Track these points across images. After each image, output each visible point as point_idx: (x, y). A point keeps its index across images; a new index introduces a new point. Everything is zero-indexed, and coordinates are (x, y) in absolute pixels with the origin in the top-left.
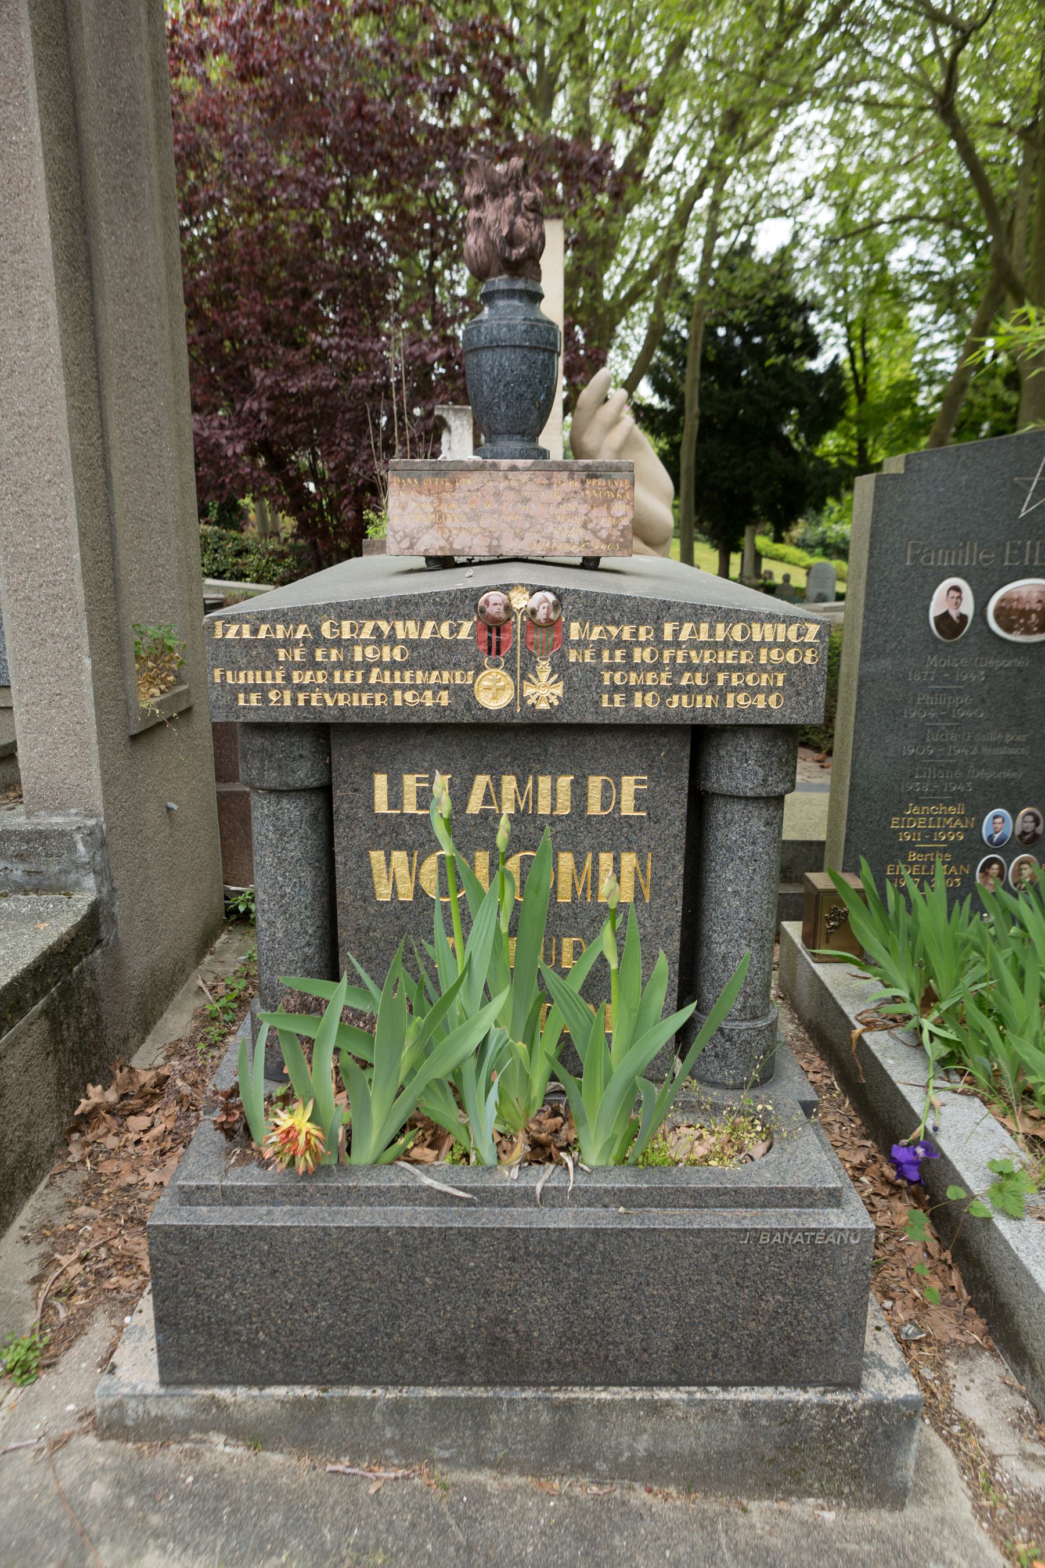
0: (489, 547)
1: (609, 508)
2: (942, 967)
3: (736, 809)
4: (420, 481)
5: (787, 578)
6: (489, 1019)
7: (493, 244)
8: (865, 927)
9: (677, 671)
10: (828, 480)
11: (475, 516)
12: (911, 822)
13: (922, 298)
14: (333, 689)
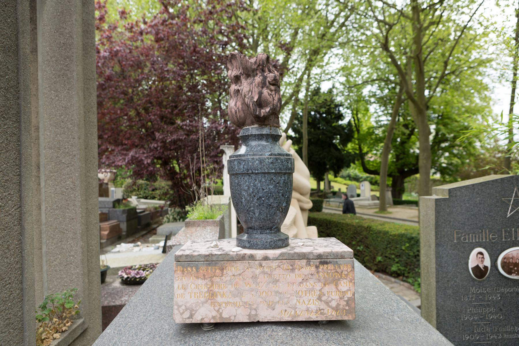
0: (249, 315)
1: (337, 285)
4: (197, 269)
5: (340, 190)
7: (248, 106)
10: (351, 158)
11: (239, 294)
13: (374, 102)
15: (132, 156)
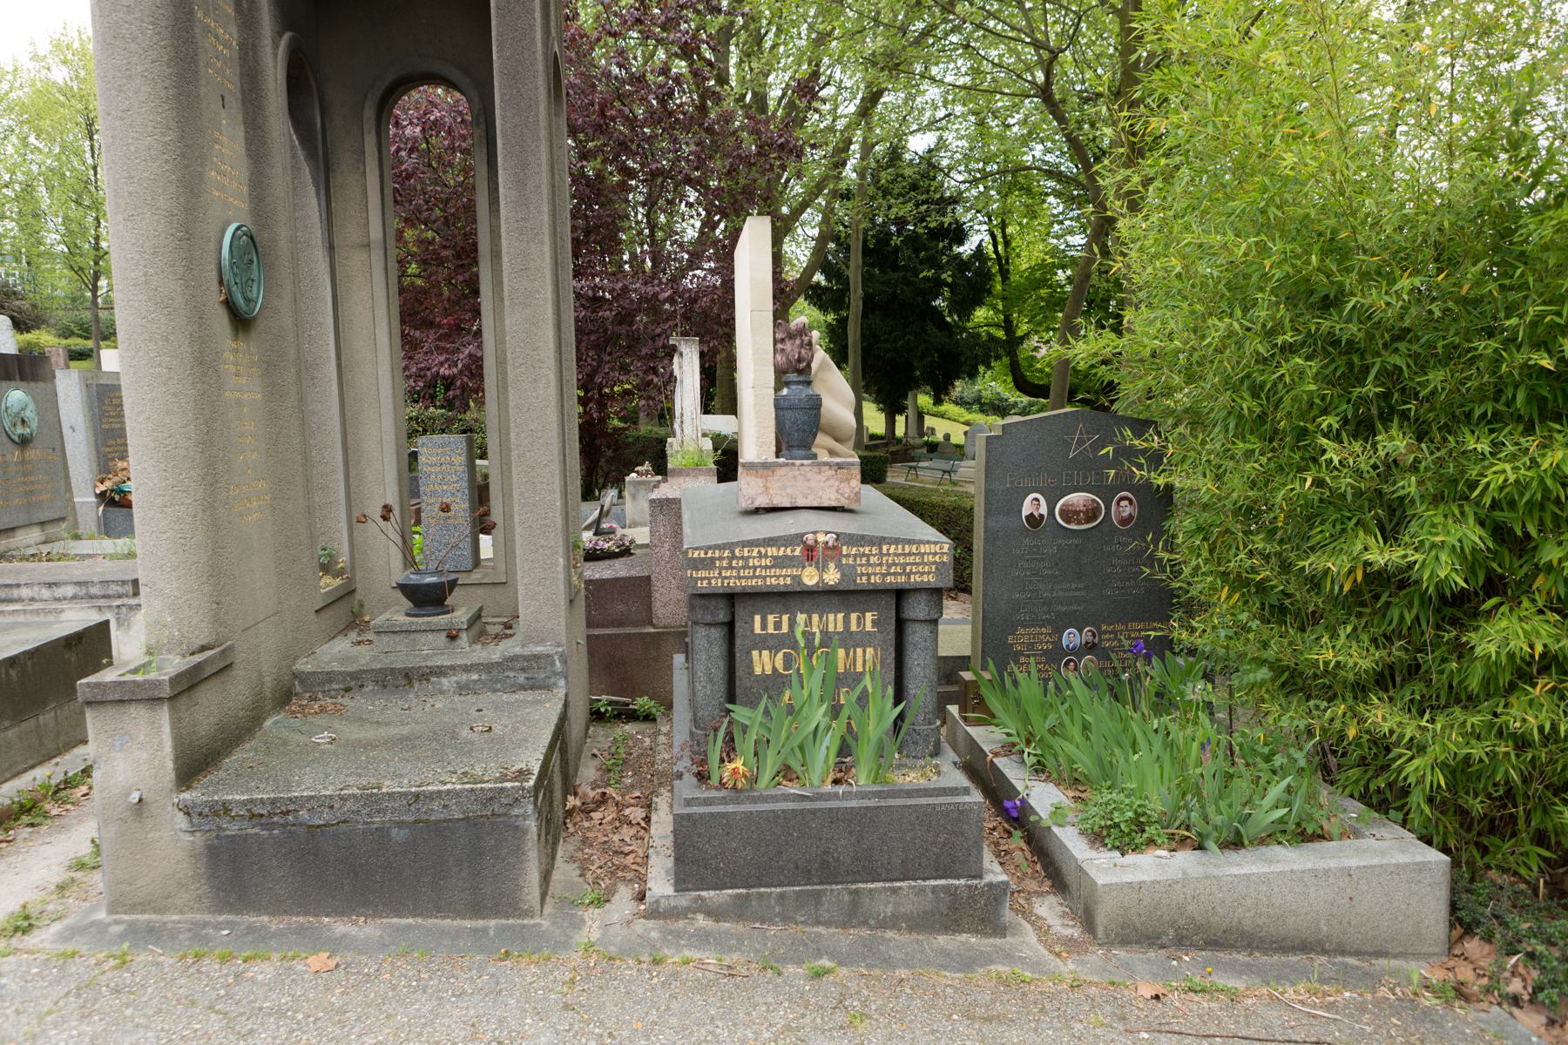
2: (1035, 718)
3: (917, 626)
5: (947, 437)
6: (819, 714)
8: (994, 702)
9: (889, 566)
11: (784, 488)
12: (1020, 638)
14: (740, 578)
15: (470, 355)
